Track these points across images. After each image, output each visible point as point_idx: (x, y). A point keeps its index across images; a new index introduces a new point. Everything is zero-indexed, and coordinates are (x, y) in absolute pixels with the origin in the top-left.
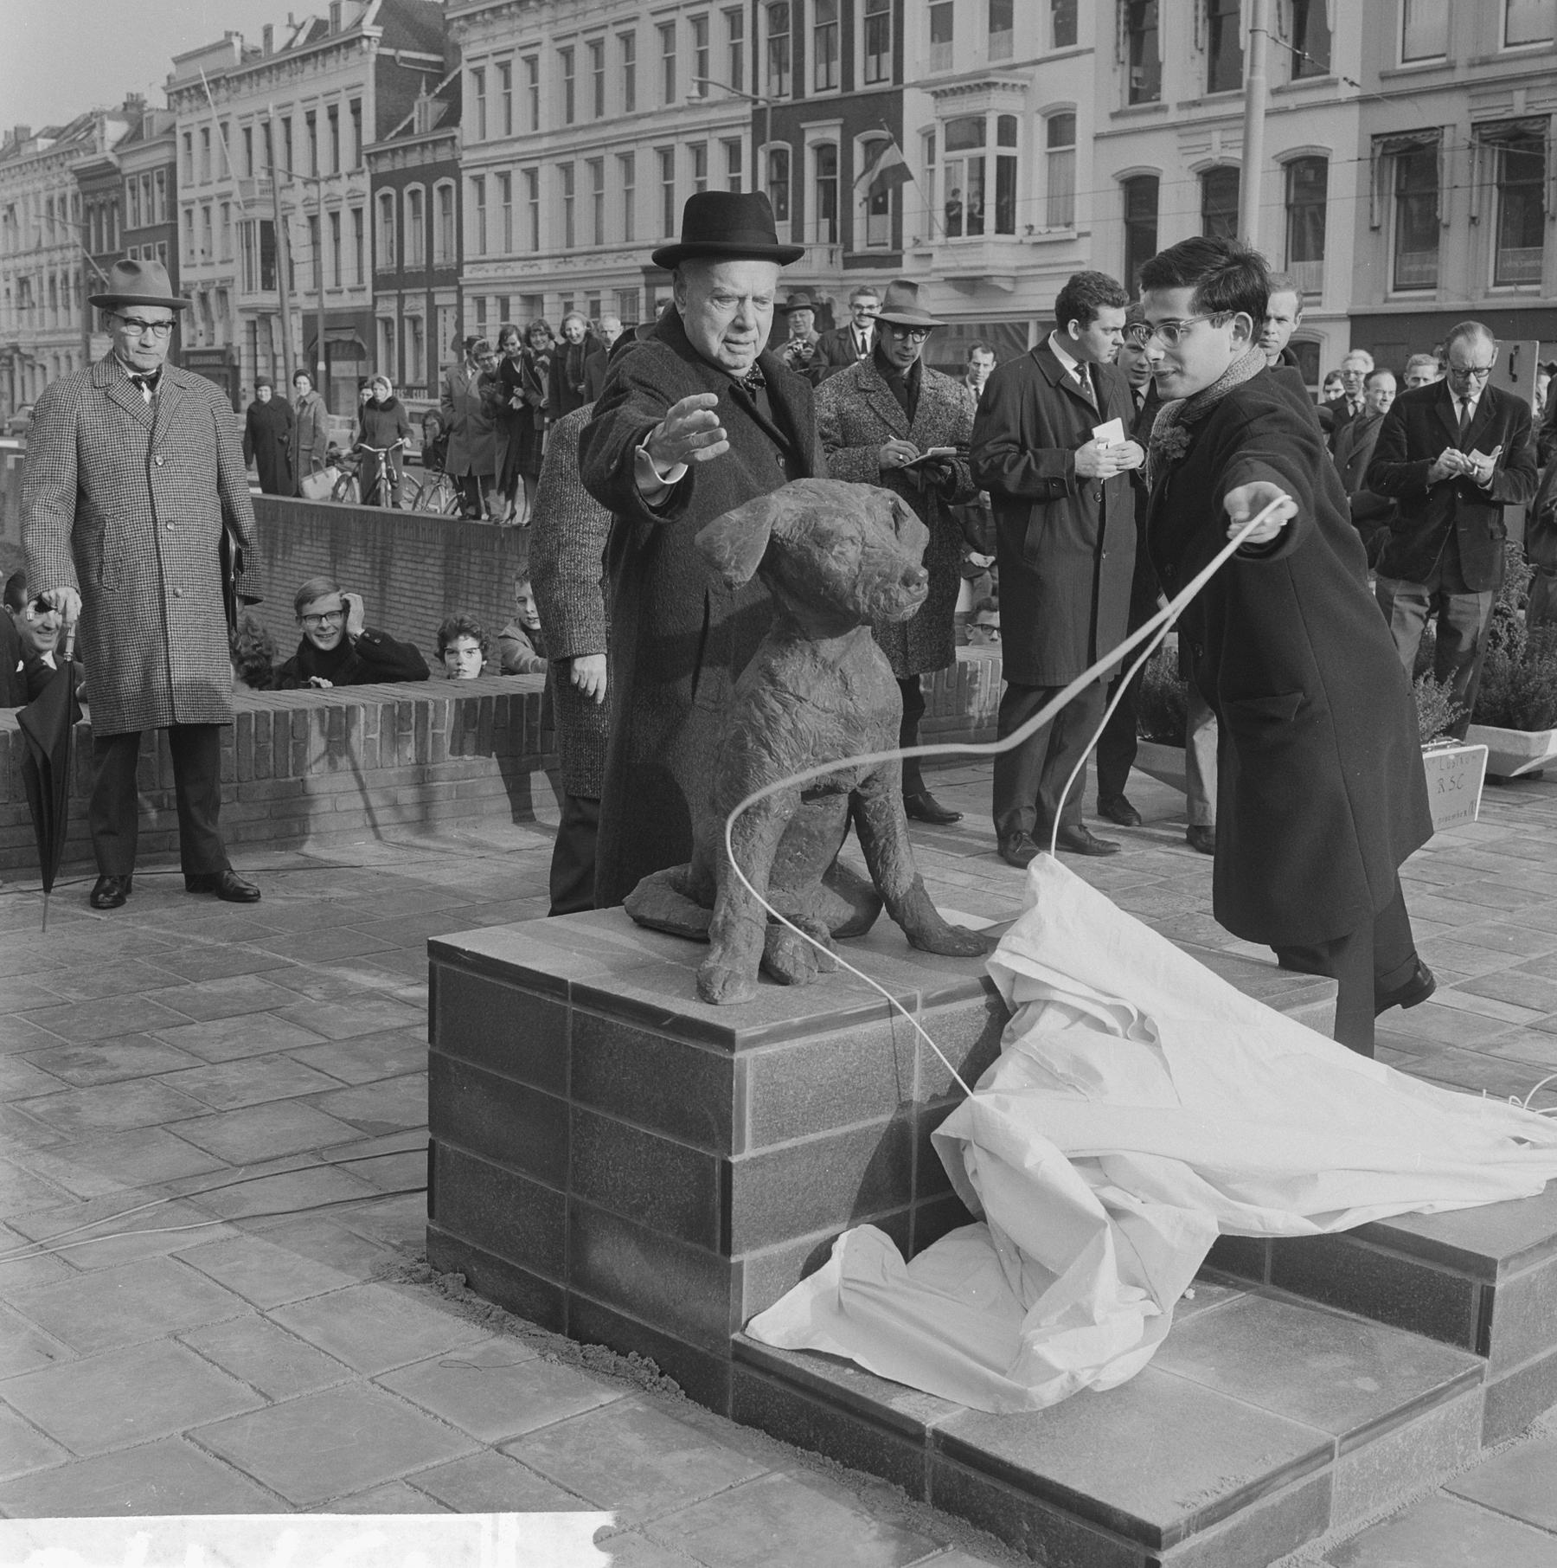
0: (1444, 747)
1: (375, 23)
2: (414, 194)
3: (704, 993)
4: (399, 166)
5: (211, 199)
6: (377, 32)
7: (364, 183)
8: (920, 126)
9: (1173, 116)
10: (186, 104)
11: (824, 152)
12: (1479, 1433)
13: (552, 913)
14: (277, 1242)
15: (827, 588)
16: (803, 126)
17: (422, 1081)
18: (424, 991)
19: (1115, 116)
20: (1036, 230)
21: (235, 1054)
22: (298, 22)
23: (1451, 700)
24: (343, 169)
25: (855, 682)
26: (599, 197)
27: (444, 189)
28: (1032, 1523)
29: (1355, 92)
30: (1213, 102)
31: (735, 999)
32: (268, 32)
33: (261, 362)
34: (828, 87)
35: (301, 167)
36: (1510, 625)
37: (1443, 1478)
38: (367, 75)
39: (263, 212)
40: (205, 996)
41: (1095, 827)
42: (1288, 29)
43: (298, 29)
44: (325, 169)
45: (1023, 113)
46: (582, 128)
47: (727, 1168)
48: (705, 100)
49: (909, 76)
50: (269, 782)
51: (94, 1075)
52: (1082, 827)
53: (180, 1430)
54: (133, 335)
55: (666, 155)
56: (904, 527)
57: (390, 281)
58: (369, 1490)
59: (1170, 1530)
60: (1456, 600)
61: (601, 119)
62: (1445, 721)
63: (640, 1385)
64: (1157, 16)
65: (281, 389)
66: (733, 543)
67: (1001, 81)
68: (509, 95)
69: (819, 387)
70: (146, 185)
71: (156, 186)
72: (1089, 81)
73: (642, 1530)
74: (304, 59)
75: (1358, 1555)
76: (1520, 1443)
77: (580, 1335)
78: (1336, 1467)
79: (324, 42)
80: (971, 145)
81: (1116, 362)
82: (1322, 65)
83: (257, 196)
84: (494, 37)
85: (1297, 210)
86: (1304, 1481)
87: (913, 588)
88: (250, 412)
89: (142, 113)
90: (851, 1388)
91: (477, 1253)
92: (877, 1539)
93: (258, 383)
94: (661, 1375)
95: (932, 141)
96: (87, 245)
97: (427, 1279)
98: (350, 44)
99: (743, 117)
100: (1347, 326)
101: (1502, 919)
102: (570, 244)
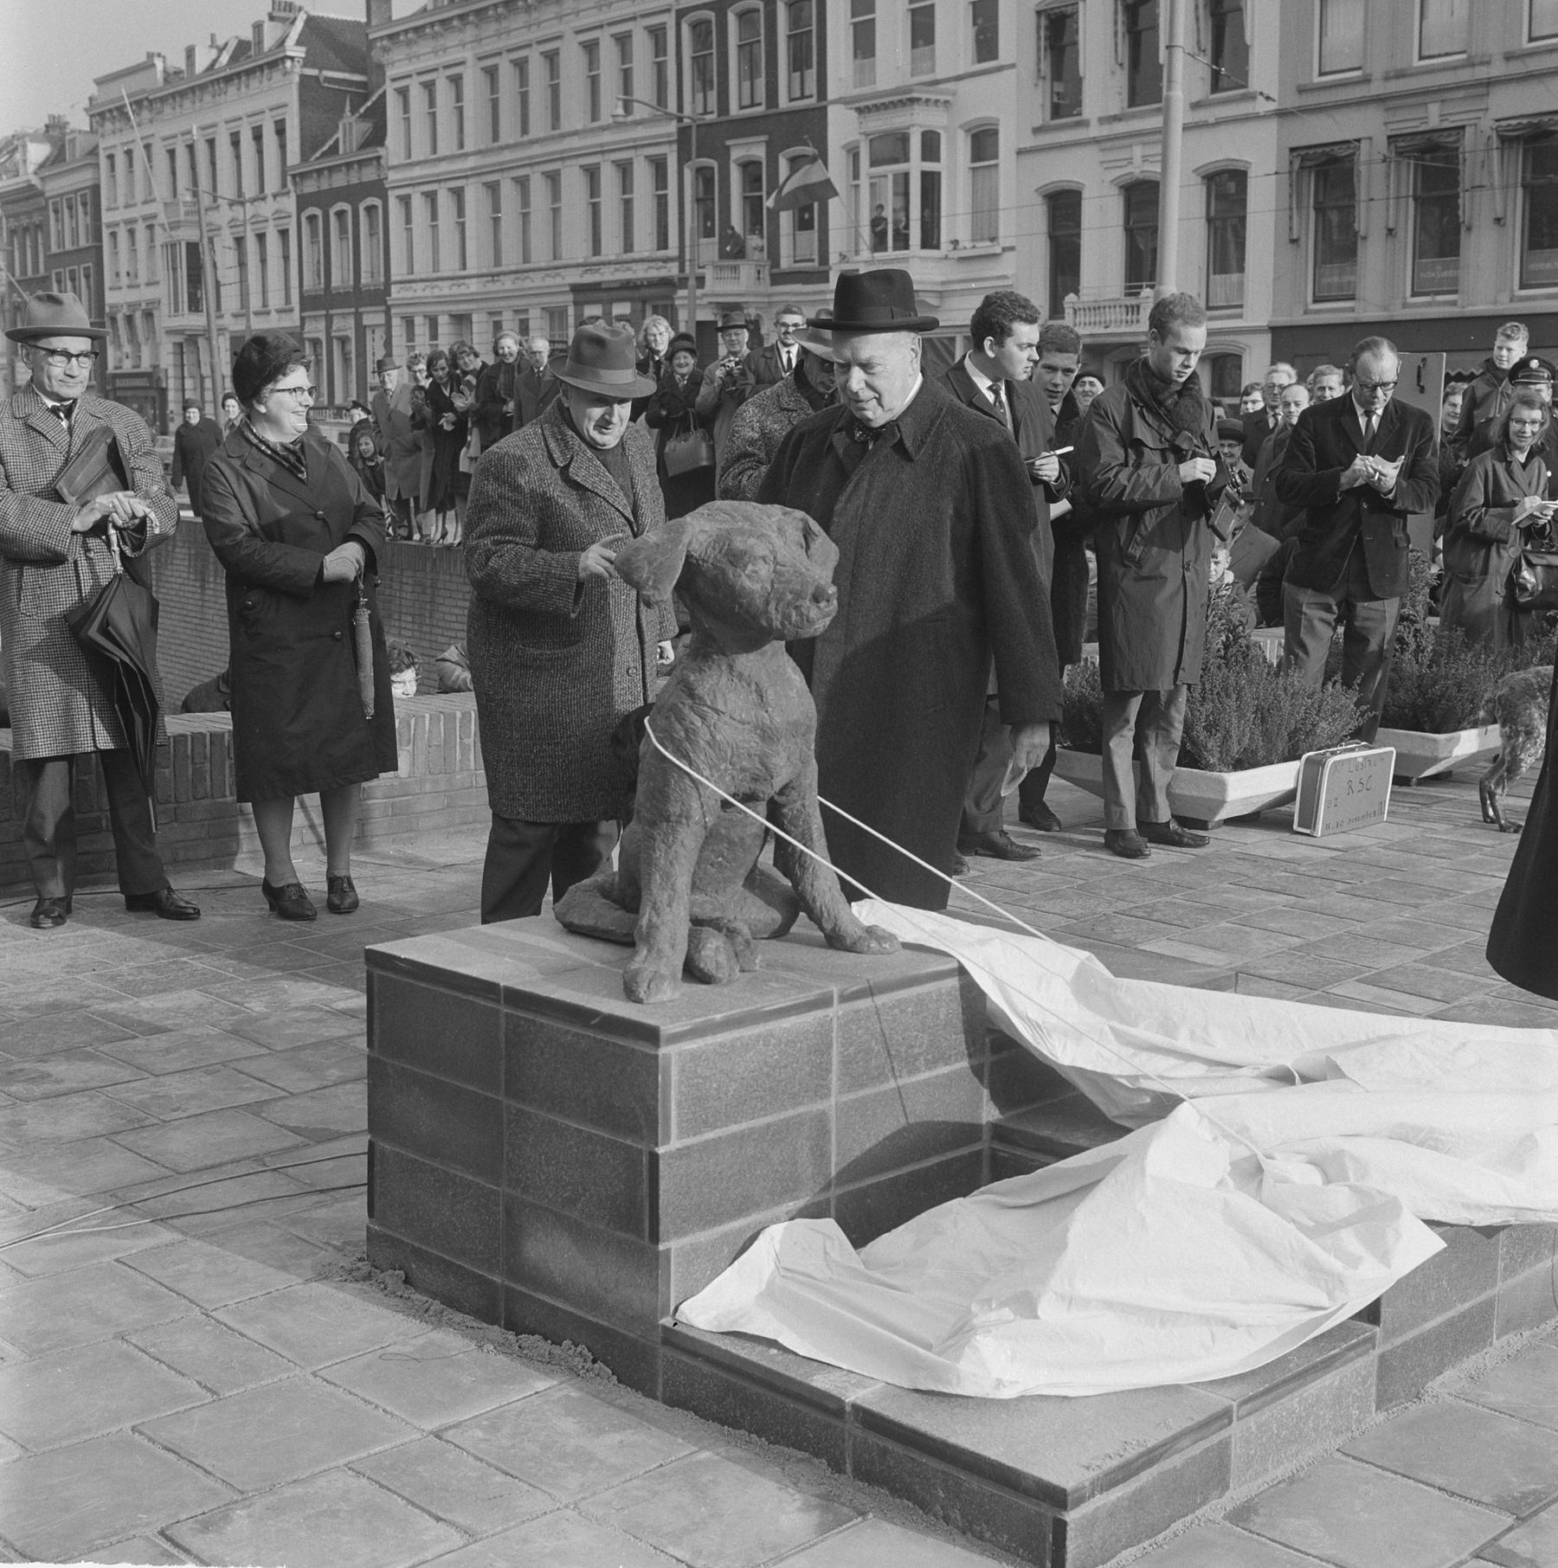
0: (1353, 750)
1: (299, 43)
2: (341, 214)
3: (630, 994)
4: (325, 186)
5: (135, 221)
6: (300, 52)
7: (290, 204)
8: (844, 142)
9: (1095, 131)
10: (108, 126)
11: (750, 169)
12: (1374, 1397)
13: (484, 922)
14: (221, 1245)
15: (741, 606)
16: (728, 143)
17: (362, 1088)
18: (362, 1001)
19: (1037, 131)
20: (961, 246)
21: (178, 1066)
22: (220, 42)
23: (1357, 705)
24: (269, 190)
25: (770, 695)
26: (525, 216)
27: (371, 210)
28: (946, 1489)
29: (1272, 106)
30: (1133, 116)
31: (659, 998)
32: (190, 53)
33: (189, 383)
34: (753, 105)
35: (226, 189)
36: (1417, 630)
37: (1339, 1441)
38: (292, 97)
39: (188, 234)
40: (147, 1011)
41: (1016, 833)
42: (1207, 43)
43: (221, 50)
44: (250, 190)
45: (944, 128)
46: (508, 147)
47: (654, 1158)
48: (630, 118)
49: (832, 94)
50: (204, 802)
51: (38, 1090)
52: (1003, 833)
53: (127, 1426)
54: (57, 366)
55: (592, 173)
56: (815, 546)
57: (317, 302)
58: (314, 1476)
59: (1076, 1490)
60: (1363, 608)
61: (526, 138)
62: (1353, 724)
63: (573, 1371)
64: (1077, 31)
65: (209, 411)
66: (650, 564)
67: (924, 96)
68: (434, 114)
69: (743, 407)
70: (70, 208)
71: (80, 208)
72: (1010, 96)
73: (576, 1507)
74: (228, 79)
75: (1257, 1514)
76: (1413, 1408)
77: (514, 1326)
78: (1235, 1430)
79: (248, 62)
80: (896, 161)
81: (1030, 378)
82: (1240, 77)
83: (182, 217)
84: (418, 57)
85: (1218, 223)
86: (1204, 1445)
87: (822, 604)
88: (178, 434)
89: (64, 135)
90: (775, 1368)
91: (417, 1252)
92: (800, 1510)
93: (186, 405)
94: (594, 1361)
95: (856, 157)
96: (11, 268)
97: (368, 1277)
98: (273, 65)
99: (669, 135)
100: (1267, 338)
101: (1407, 914)
102: (497, 262)
